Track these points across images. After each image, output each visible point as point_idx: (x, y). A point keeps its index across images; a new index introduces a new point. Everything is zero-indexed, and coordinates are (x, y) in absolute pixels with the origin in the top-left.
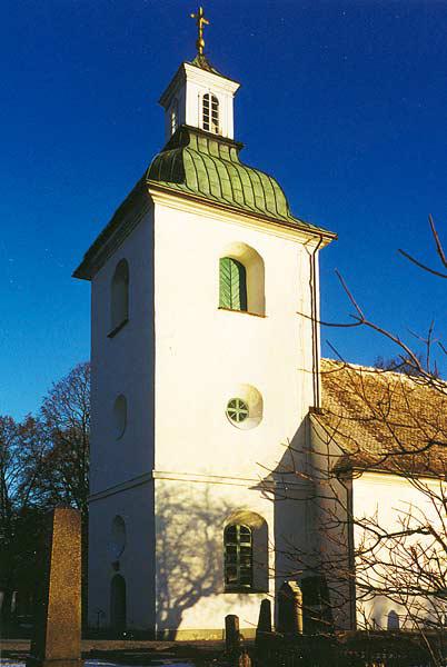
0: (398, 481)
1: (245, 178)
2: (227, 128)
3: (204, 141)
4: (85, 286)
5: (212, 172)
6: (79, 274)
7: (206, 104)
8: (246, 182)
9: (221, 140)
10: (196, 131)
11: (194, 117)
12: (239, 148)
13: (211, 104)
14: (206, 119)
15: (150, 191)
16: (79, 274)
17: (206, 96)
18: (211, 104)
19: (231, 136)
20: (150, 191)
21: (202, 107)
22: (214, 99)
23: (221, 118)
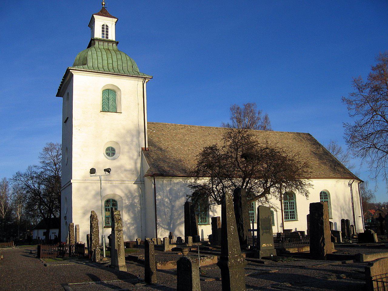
0: (324, 181)
1: (119, 57)
2: (112, 36)
3: (101, 43)
4: (61, 99)
5: (100, 58)
6: (58, 95)
7: (103, 28)
8: (115, 59)
9: (112, 42)
10: (99, 40)
11: (98, 34)
12: (117, 43)
13: (105, 29)
14: (103, 34)
15: (71, 71)
16: (58, 95)
17: (103, 25)
18: (105, 29)
19: (114, 39)
20: (71, 71)
21: (101, 32)
22: (107, 26)
23: (109, 33)
